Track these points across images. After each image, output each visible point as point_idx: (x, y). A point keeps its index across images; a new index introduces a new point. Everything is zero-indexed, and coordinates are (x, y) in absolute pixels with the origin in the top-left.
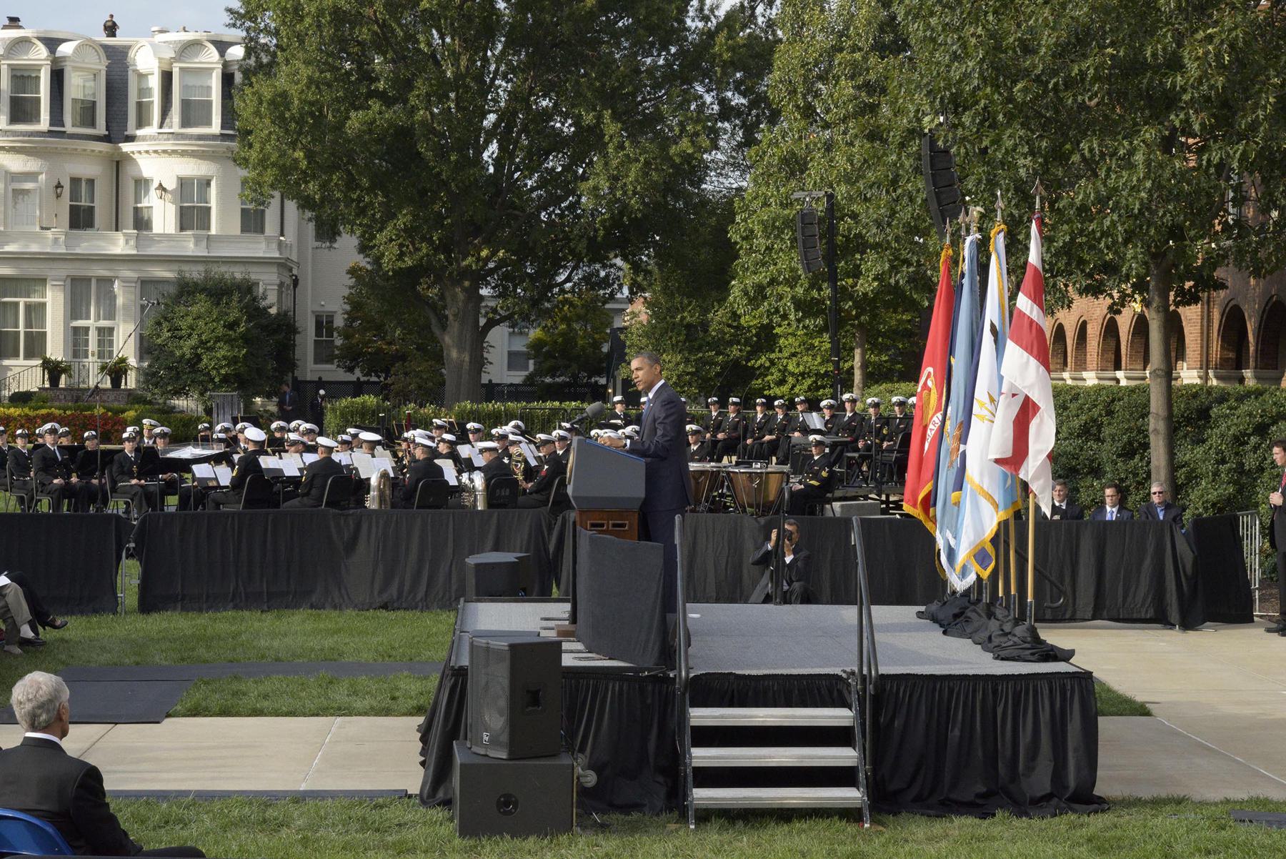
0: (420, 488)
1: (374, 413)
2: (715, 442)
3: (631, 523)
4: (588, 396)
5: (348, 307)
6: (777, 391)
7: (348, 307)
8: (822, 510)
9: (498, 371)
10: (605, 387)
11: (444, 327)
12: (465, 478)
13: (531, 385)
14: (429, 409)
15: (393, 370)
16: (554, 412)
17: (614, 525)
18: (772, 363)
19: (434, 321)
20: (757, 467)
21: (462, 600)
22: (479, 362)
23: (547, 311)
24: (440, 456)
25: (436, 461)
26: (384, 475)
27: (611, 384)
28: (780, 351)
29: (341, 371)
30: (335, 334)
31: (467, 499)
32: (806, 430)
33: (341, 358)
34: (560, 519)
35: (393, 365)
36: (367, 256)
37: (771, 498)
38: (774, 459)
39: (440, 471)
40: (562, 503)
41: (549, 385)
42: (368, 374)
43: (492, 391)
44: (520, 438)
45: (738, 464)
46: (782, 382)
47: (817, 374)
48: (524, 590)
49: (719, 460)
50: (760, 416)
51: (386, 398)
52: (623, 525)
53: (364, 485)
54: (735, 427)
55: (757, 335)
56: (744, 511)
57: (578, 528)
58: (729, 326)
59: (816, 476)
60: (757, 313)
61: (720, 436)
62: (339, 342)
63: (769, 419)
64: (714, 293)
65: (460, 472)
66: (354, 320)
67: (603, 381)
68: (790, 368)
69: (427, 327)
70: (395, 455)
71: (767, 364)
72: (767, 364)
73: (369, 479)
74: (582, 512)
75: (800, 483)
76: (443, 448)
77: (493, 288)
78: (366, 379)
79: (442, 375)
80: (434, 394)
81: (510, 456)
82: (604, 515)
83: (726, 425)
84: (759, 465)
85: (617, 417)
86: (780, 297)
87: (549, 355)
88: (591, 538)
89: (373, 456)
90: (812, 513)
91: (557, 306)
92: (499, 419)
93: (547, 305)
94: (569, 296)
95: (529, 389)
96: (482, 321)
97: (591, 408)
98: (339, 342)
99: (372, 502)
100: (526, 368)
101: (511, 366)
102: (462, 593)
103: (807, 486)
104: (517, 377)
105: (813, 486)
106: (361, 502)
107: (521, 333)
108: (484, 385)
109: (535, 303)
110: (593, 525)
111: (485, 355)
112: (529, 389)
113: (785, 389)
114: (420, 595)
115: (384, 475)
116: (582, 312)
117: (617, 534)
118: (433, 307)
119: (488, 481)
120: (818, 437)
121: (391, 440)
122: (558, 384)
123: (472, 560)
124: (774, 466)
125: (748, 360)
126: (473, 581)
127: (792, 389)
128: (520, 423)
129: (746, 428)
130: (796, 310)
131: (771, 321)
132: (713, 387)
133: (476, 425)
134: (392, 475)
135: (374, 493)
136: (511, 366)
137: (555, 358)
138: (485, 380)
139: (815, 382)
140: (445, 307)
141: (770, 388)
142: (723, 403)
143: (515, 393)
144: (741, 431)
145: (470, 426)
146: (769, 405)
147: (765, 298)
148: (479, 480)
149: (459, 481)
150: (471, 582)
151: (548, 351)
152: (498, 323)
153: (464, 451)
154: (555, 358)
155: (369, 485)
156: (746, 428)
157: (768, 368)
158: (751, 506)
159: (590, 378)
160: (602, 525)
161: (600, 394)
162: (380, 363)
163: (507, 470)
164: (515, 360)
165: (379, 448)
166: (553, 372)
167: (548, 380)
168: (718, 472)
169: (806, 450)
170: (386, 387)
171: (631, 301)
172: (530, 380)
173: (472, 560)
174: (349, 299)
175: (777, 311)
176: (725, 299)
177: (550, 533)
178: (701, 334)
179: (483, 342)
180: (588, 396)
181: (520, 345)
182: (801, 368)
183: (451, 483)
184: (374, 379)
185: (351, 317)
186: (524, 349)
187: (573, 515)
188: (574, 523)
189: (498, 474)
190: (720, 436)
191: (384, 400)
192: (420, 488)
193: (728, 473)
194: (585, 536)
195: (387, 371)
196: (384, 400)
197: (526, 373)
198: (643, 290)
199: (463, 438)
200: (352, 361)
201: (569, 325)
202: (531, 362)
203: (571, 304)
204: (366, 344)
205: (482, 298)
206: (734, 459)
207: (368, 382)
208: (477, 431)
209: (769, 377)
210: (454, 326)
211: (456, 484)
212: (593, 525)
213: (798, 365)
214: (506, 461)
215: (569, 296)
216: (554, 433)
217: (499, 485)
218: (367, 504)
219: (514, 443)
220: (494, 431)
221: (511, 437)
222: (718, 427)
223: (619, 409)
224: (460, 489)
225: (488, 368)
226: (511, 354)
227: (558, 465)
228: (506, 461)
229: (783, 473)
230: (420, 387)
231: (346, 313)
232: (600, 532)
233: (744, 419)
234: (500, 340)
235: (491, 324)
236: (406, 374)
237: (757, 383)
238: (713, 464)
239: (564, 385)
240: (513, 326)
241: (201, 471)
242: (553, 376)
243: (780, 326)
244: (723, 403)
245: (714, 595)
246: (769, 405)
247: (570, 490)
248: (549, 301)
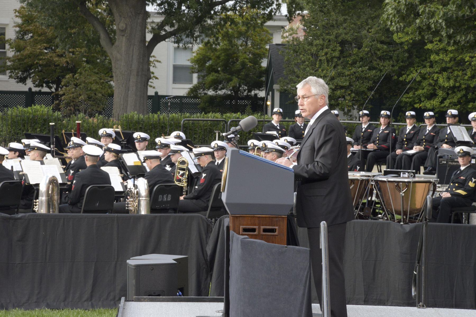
0: (86, 192)
1: (46, 121)
2: (365, 153)
3: (281, 229)
4: (248, 108)
5: (19, 21)
6: (428, 104)
7: (19, 21)
8: (468, 219)
9: (165, 84)
10: (264, 100)
11: (112, 41)
12: (130, 183)
13: (196, 97)
14: (95, 121)
15: (64, 82)
16: (216, 123)
17: (265, 230)
18: (424, 78)
19: (102, 35)
20: (405, 177)
21: (123, 299)
22: (146, 76)
23: (210, 28)
24: (105, 163)
25: (103, 168)
26: (53, 181)
27: (270, 97)
28: (431, 66)
29: (13, 81)
30: (7, 46)
31: (131, 204)
32: (453, 142)
33: (13, 69)
34: (218, 222)
35: (63, 77)
36: (327, 39)
37: (418, 205)
38: (422, 168)
39: (106, 178)
40: (218, 209)
41: (212, 98)
42: (40, 85)
43: (157, 102)
44: (181, 147)
45: (386, 173)
46: (432, 96)
47: (468, 88)
48: (182, 290)
49: (370, 170)
50: (409, 128)
51: (57, 108)
52: (273, 231)
53: (33, 190)
54: (385, 138)
55: (408, 51)
56: (393, 217)
57: (231, 232)
58: (382, 42)
59: (463, 185)
60: (410, 30)
61: (371, 147)
62: (10, 53)
63: (417, 131)
64: (368, 11)
65: (125, 178)
66: (25, 33)
67: (262, 94)
68: (441, 81)
69: (97, 41)
70: (63, 162)
71: (419, 79)
72: (419, 79)
73: (37, 185)
74: (235, 218)
75: (447, 191)
76: (109, 157)
77: (159, 5)
78: (37, 89)
79: (110, 87)
80: (101, 105)
81: (172, 165)
82: (258, 224)
83: (376, 135)
84: (406, 175)
85: (273, 128)
86: (432, 14)
87: (212, 69)
88: (243, 242)
89: (42, 163)
90: (459, 221)
91: (219, 24)
92: (165, 130)
93: (209, 22)
94: (229, 13)
95: (193, 101)
96: (149, 37)
97: (246, 120)
98: (10, 53)
99: (41, 206)
100: (191, 81)
101: (176, 80)
102: (124, 293)
103: (454, 195)
104: (182, 90)
105: (459, 195)
106: (30, 207)
107: (185, 48)
108: (150, 97)
109: (199, 20)
110: (245, 230)
111: (152, 69)
112: (193, 101)
113: (435, 102)
114: (86, 296)
115: (53, 181)
116: (243, 29)
117: (267, 240)
118: (102, 23)
119: (151, 187)
120: (465, 148)
121: (59, 149)
122: (220, 96)
123: (133, 262)
124: (421, 176)
125: (400, 75)
126: (134, 282)
127: (442, 102)
128: (182, 134)
129: (395, 140)
130: (448, 27)
131: (423, 37)
132: (365, 99)
133: (143, 135)
134: (60, 181)
135: (43, 198)
136: (176, 80)
137: (217, 72)
138: (151, 92)
139: (465, 96)
140: (112, 22)
141: (420, 101)
142: (374, 116)
143: (179, 104)
144: (390, 142)
145: (136, 135)
146: (419, 118)
147: (417, 15)
148: (142, 184)
149: (125, 187)
150: (131, 282)
151: (211, 66)
152: (163, 38)
153: (130, 159)
154: (217, 72)
155: (38, 190)
156: (395, 140)
157: (420, 82)
158: (399, 213)
159: (250, 91)
160: (254, 230)
161: (258, 106)
162: (52, 74)
163: (169, 177)
164: (179, 73)
165: (49, 156)
166: (215, 85)
167: (211, 93)
168: (368, 181)
169: (453, 160)
170: (57, 97)
171: (290, 18)
172: (194, 92)
173: (133, 262)
174: (20, 13)
175: (429, 27)
176: (378, 16)
177: (207, 237)
178: (355, 50)
179: (149, 56)
180: (248, 108)
181: (185, 59)
182: (452, 83)
183: (116, 190)
184: (45, 89)
185: (22, 32)
186: (189, 63)
187: (227, 221)
188: (228, 228)
189: (161, 184)
190: (371, 147)
191: (54, 110)
192: (86, 192)
193: (377, 182)
194: (237, 240)
195: (58, 82)
196: (54, 110)
197: (190, 86)
198: (302, 9)
199: (129, 146)
200: (23, 72)
201: (230, 42)
202: (195, 76)
203: (233, 22)
204: (37, 56)
205: (147, 15)
206: (384, 168)
207: (40, 93)
208: (144, 139)
209: (420, 92)
210: (121, 41)
211: (121, 190)
212: (245, 230)
213: (449, 79)
214: (168, 168)
215: (229, 13)
216: (213, 144)
217: (161, 191)
218: (36, 209)
219: (175, 152)
220: (157, 140)
221: (173, 147)
222: (368, 138)
223: (275, 120)
224: (125, 194)
225: (153, 82)
226: (176, 68)
227: (214, 173)
228: (168, 168)
229: (430, 182)
230: (89, 98)
231: (18, 26)
232: (252, 236)
233: (394, 131)
234: (166, 56)
235: (157, 39)
236: (76, 85)
237: (405, 98)
238: (363, 173)
239: (226, 97)
240: (178, 42)
241: (443, 162)
242: (215, 89)
243: (432, 42)
244: (374, 116)
245: (363, 297)
246: (419, 118)
247: (224, 197)
248: (211, 18)
